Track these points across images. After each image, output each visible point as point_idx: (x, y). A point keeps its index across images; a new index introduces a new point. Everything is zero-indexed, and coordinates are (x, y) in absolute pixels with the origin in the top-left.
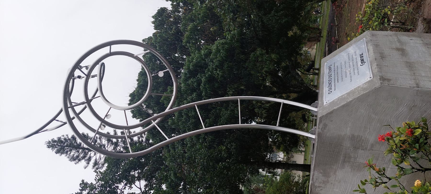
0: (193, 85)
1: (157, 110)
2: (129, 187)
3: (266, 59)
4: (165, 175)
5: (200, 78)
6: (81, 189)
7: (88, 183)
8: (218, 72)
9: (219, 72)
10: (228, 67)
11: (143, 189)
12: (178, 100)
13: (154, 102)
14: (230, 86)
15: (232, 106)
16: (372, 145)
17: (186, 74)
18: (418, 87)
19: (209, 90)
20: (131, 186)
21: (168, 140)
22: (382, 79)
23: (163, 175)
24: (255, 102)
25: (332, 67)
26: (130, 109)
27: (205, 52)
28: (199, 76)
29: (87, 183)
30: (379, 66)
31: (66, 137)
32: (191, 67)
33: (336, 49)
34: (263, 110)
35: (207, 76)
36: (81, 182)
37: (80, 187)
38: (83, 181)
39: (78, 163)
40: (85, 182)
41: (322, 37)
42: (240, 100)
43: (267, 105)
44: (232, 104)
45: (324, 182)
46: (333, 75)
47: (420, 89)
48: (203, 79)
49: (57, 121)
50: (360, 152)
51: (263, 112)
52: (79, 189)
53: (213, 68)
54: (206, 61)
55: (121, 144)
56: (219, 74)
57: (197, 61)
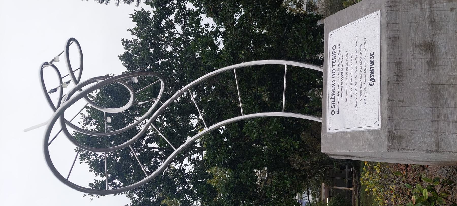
4: (244, 180)
7: (129, 40)
18: (437, 151)
23: (276, 149)
26: (46, 125)
29: (128, 41)
33: (114, 108)
38: (123, 40)
40: (126, 40)
41: (150, 13)
49: (77, 69)
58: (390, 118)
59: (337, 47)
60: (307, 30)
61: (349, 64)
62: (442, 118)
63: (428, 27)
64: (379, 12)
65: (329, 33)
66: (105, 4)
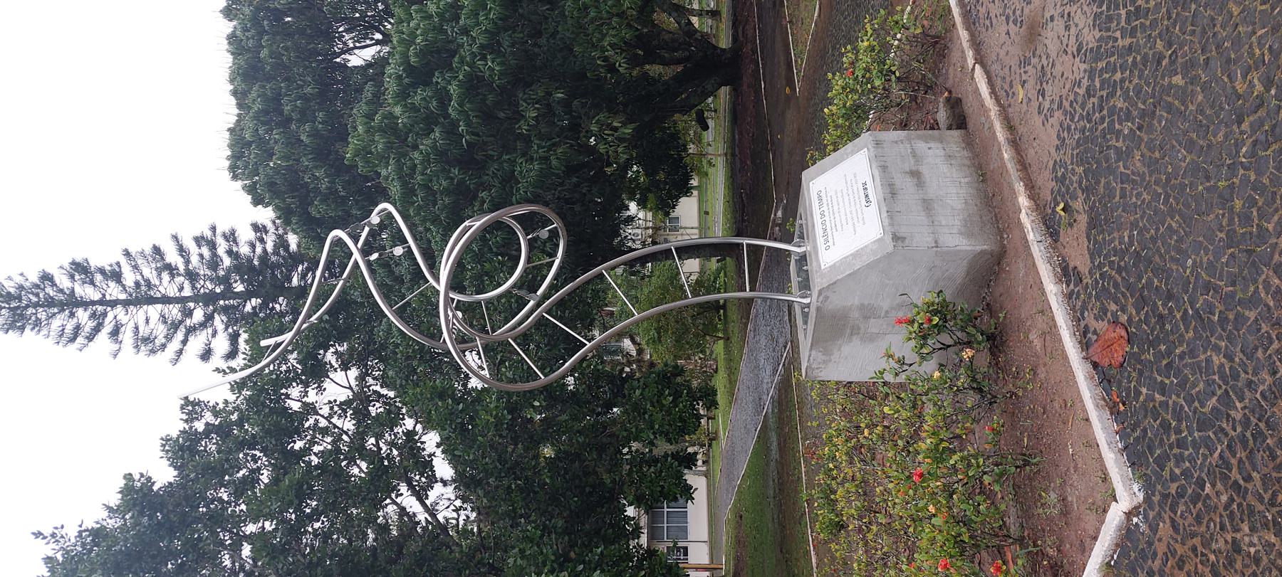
0: (427, 108)
1: (325, 177)
2: (315, 391)
3: (608, 12)
5: (443, 84)
6: (185, 417)
8: (490, 64)
9: (493, 62)
10: (513, 45)
11: (356, 389)
12: (395, 154)
13: (310, 157)
14: (526, 96)
15: (539, 147)
16: (887, 312)
17: (399, 77)
18: (937, 247)
19: (476, 117)
20: (319, 387)
21: (589, 345)
22: (896, 238)
24: (596, 129)
25: (823, 194)
27: (438, 8)
28: (439, 81)
29: (200, 401)
30: (891, 214)
31: (20, 280)
32: (412, 59)
34: (619, 146)
35: (461, 77)
36: (183, 402)
37: (183, 413)
39: (85, 346)
42: (676, 249)
43: (627, 131)
44: (538, 142)
45: (824, 362)
46: (828, 223)
47: (939, 249)
48: (453, 89)
50: (872, 320)
51: (620, 150)
52: (181, 419)
53: (473, 55)
54: (447, 32)
55: (202, 272)
56: (494, 69)
57: (427, 40)
58: (891, 225)
59: (823, 192)
60: (660, 387)
61: (840, 199)
62: (936, 223)
63: (912, 161)
64: (866, 150)
65: (811, 183)
66: (77, 349)
